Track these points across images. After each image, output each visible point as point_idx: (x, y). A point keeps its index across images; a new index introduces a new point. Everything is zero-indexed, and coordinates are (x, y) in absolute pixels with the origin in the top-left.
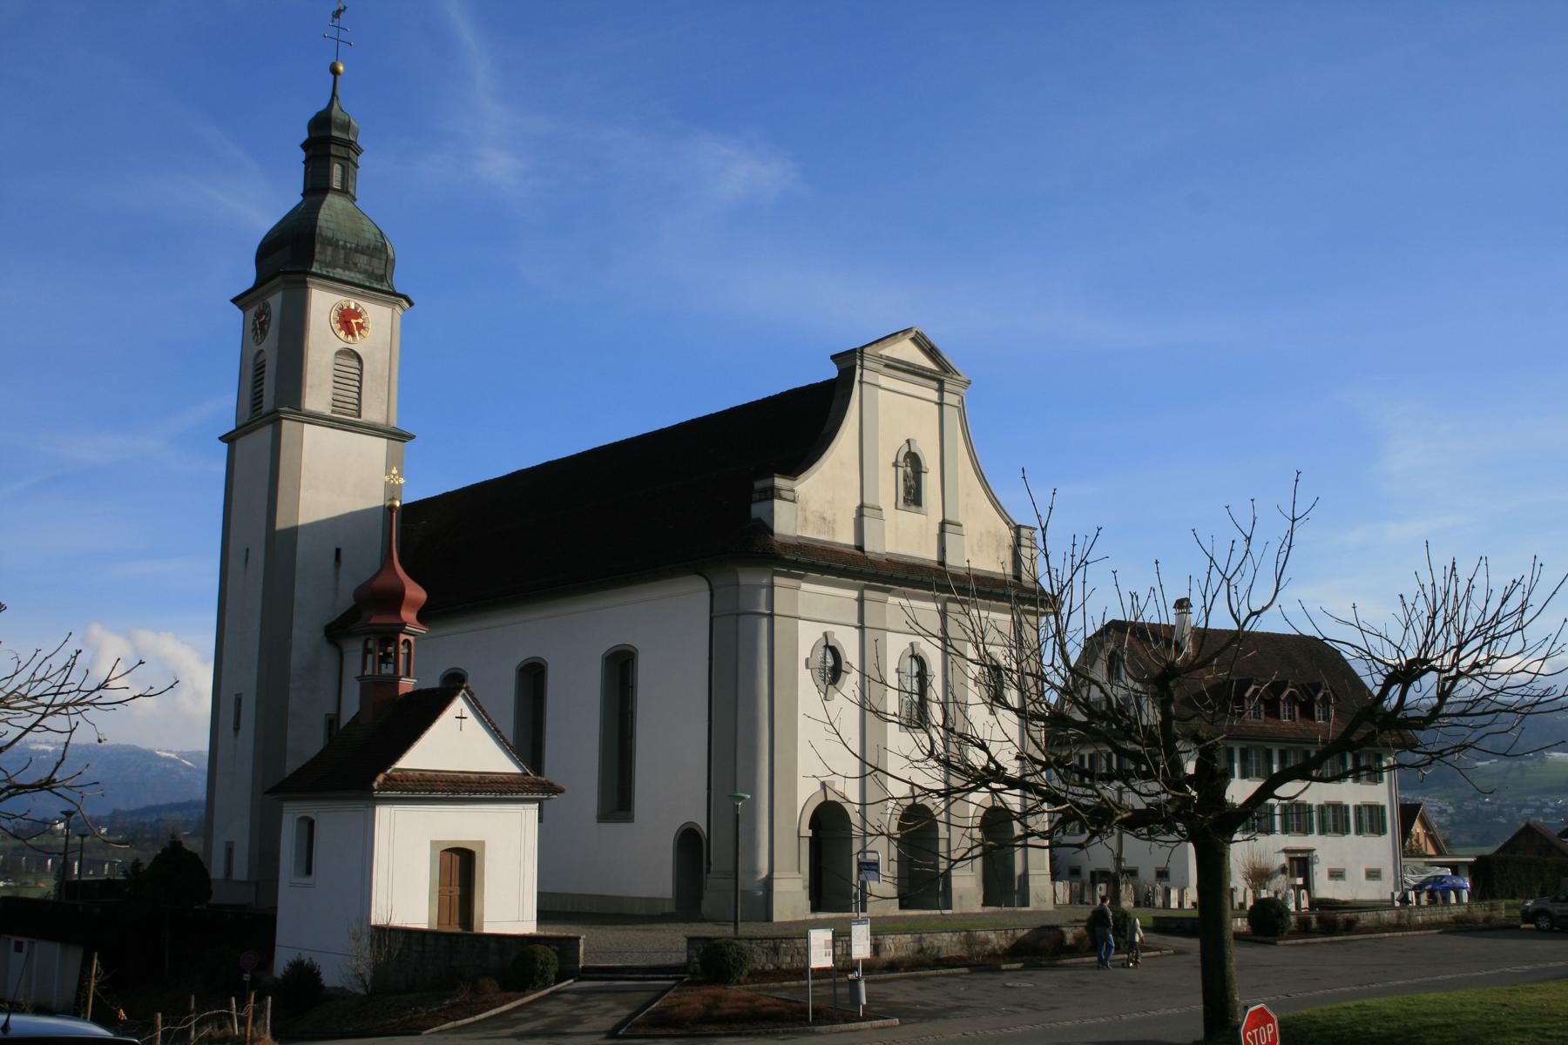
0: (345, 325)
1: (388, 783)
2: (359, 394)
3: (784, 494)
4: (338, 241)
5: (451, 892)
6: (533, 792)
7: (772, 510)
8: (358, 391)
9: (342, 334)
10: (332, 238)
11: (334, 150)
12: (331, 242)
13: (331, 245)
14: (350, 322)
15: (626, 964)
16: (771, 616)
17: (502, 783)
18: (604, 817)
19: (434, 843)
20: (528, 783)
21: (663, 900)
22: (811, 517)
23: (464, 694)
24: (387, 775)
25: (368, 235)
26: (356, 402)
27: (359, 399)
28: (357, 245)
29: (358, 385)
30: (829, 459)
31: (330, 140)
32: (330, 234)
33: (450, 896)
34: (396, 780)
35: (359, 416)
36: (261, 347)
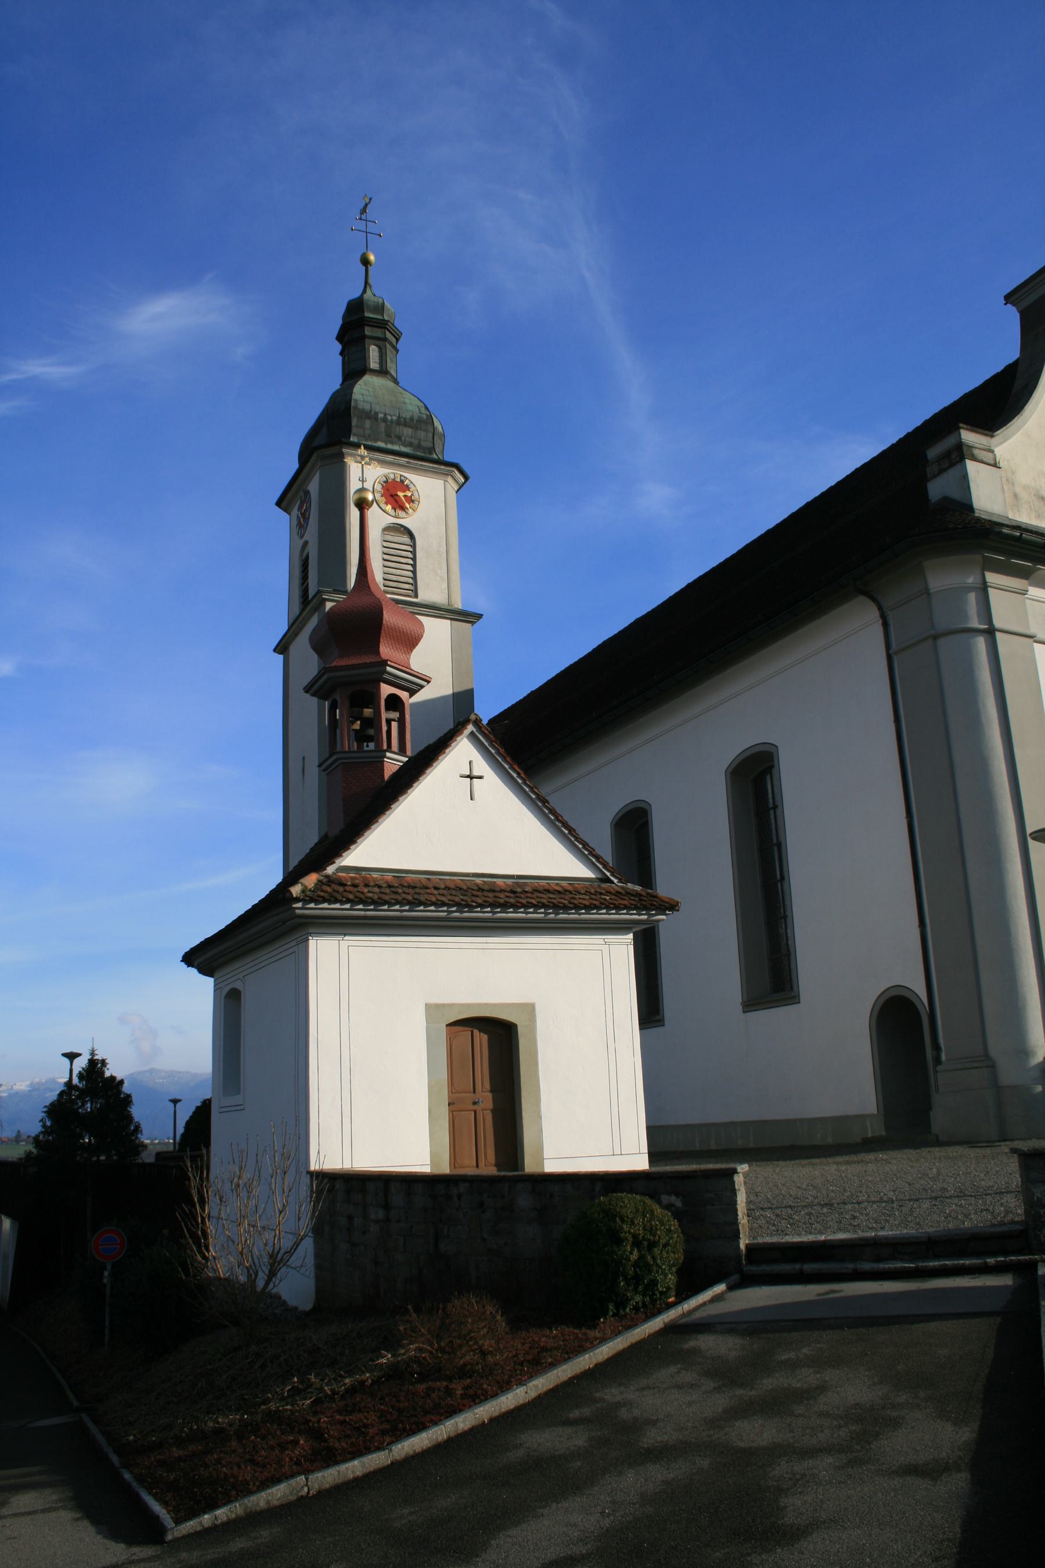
0: (392, 499)
1: (326, 888)
2: (414, 572)
3: (978, 453)
4: (376, 413)
5: (475, 1103)
6: (618, 908)
7: (965, 477)
8: (412, 569)
9: (389, 508)
10: (371, 411)
11: (368, 331)
12: (370, 415)
13: (370, 418)
14: (397, 495)
15: (861, 1234)
16: (990, 632)
17: (559, 892)
18: (751, 1003)
19: (432, 1010)
20: (609, 893)
21: (862, 1118)
22: (1024, 495)
23: (472, 733)
24: (327, 876)
25: (410, 408)
26: (411, 581)
27: (415, 578)
28: (399, 417)
29: (412, 562)
30: (1034, 416)
31: (363, 322)
32: (367, 407)
33: (475, 1112)
34: (344, 885)
35: (416, 596)
36: (305, 539)
